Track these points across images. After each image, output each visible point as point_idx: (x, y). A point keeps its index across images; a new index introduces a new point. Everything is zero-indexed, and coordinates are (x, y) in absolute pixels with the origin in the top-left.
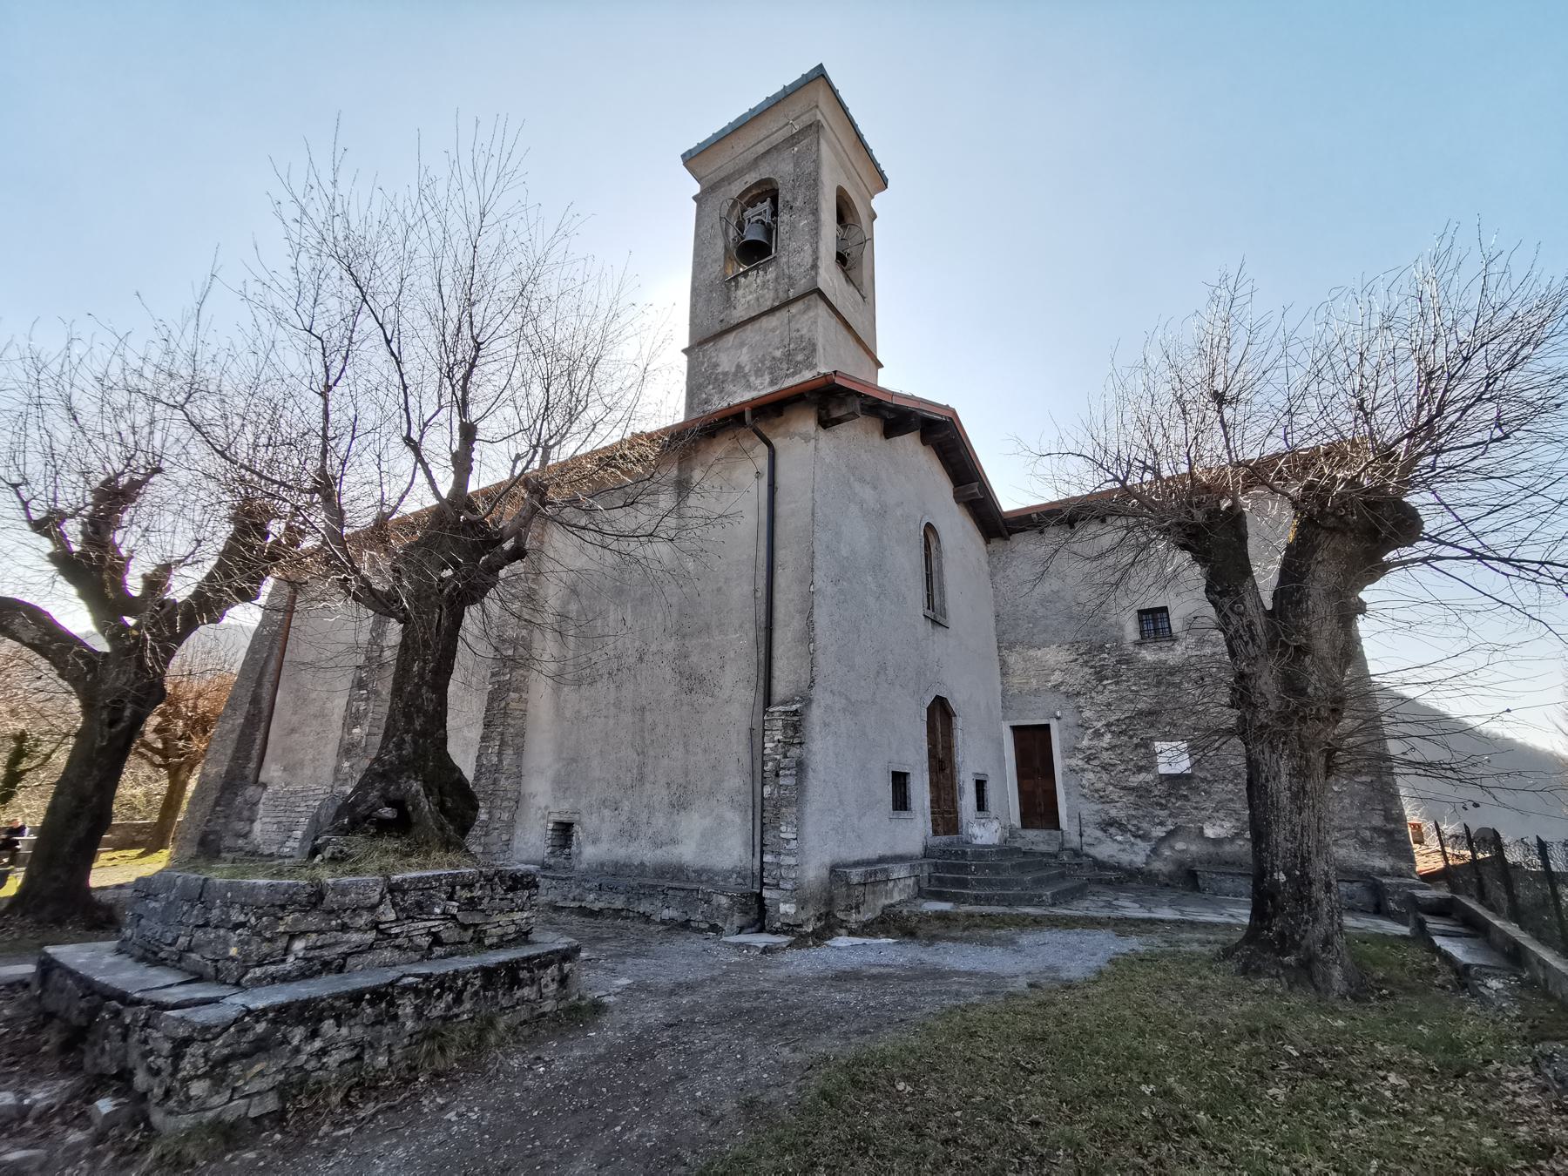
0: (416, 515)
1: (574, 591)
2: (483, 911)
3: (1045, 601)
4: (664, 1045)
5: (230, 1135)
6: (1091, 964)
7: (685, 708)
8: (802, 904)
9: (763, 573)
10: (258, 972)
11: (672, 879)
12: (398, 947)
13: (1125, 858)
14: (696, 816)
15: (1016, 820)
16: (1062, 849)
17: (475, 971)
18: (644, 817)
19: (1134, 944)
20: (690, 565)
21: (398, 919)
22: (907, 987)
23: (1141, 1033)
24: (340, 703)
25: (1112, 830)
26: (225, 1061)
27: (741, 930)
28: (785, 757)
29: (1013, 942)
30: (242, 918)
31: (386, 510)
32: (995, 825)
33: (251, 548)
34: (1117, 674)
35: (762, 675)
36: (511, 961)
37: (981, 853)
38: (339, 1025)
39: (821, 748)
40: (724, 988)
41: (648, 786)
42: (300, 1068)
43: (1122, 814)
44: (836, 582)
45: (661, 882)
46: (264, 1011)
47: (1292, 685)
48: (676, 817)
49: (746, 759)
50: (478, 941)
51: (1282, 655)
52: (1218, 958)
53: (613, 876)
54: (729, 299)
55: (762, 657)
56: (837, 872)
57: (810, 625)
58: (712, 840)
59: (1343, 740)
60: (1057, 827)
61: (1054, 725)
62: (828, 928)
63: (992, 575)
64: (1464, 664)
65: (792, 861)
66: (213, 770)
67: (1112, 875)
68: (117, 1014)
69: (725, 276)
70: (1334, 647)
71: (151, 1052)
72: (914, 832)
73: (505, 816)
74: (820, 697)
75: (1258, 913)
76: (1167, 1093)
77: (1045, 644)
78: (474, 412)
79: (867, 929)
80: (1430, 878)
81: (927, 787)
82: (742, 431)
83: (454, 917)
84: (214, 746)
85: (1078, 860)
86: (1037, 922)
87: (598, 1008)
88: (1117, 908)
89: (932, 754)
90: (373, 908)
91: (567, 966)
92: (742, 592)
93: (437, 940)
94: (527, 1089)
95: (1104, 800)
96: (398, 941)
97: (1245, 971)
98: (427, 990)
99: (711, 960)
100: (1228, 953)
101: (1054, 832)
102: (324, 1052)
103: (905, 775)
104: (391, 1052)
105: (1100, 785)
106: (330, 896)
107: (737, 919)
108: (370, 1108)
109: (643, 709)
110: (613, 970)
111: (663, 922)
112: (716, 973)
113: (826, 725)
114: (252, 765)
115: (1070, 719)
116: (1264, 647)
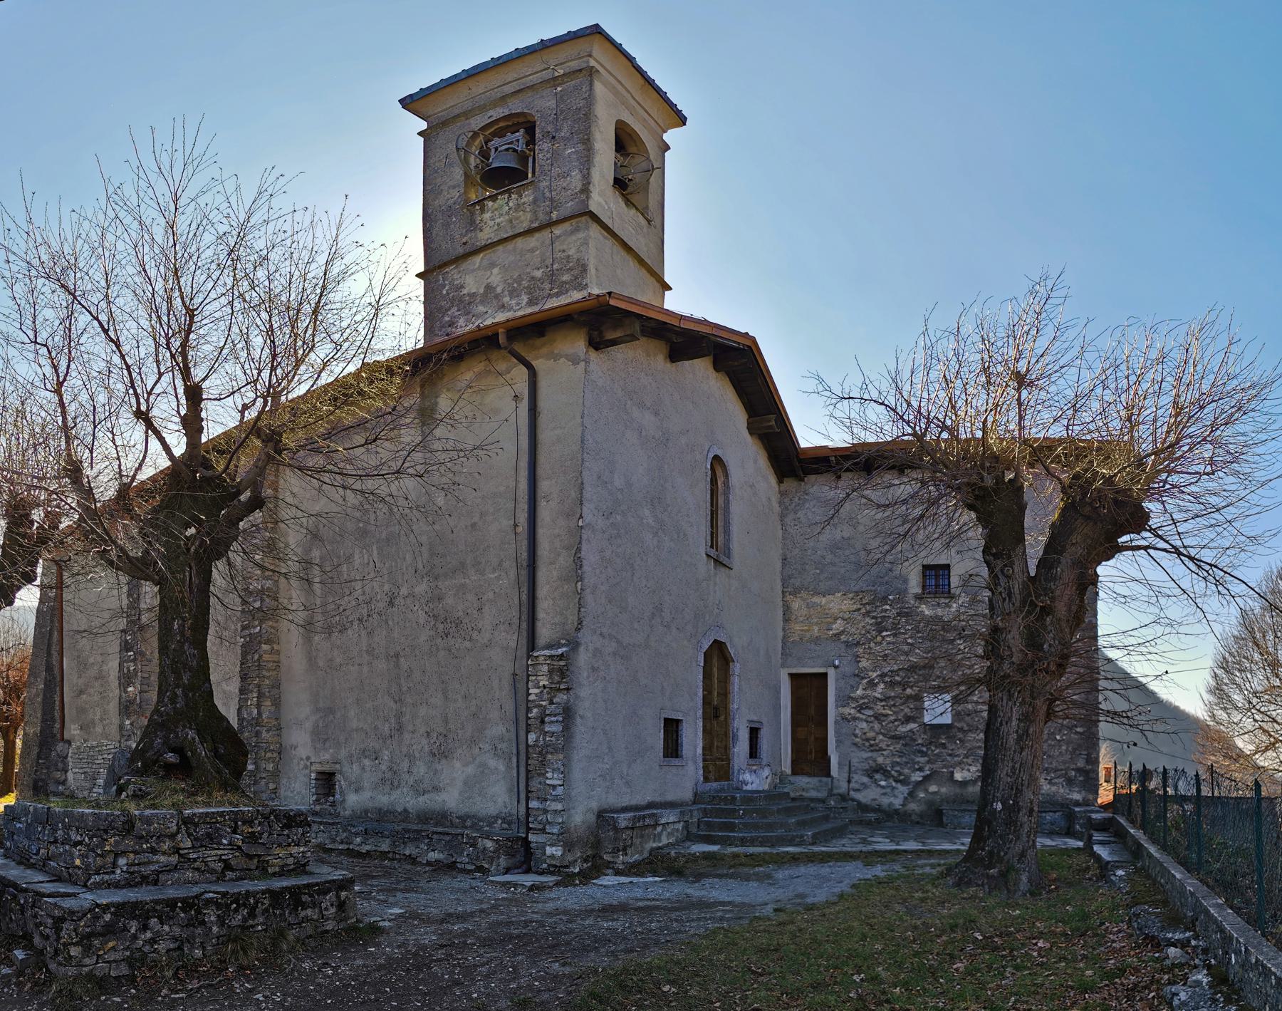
0: (153, 479)
1: (315, 536)
2: (263, 844)
3: (834, 547)
4: (439, 960)
5: (102, 984)
6: (835, 890)
7: (442, 653)
8: (569, 847)
9: (524, 505)
10: (98, 878)
11: (436, 825)
12: (198, 869)
13: (885, 801)
14: (458, 764)
15: (787, 768)
16: (831, 794)
17: (263, 892)
18: (405, 765)
19: (879, 871)
20: (440, 500)
21: (193, 847)
22: (673, 916)
23: (864, 937)
24: (113, 665)
25: (878, 776)
26: (89, 936)
27: (507, 871)
28: (551, 703)
29: (769, 876)
30: (79, 838)
31: (125, 480)
32: (767, 772)
33: (24, 536)
34: (895, 627)
35: (524, 617)
36: (293, 887)
37: (751, 797)
38: (162, 924)
39: (588, 695)
40: (493, 918)
41: (407, 736)
42: (140, 950)
43: (888, 761)
44: (608, 515)
45: (425, 827)
46: (108, 906)
47: (1033, 640)
48: (439, 767)
49: (509, 707)
50: (263, 870)
51: (1029, 613)
52: (942, 875)
53: (377, 821)
54: (472, 222)
55: (524, 597)
56: (604, 817)
57: (578, 562)
58: (474, 784)
59: (1062, 691)
60: (828, 775)
61: (832, 674)
62: (595, 868)
63: (782, 517)
64: (1148, 633)
65: (559, 807)
66: (31, 731)
67: (872, 816)
68: (15, 897)
69: (466, 201)
70: (1069, 610)
71: (41, 924)
72: (687, 777)
73: (270, 767)
74: (588, 639)
75: (978, 839)
76: (875, 979)
77: (830, 592)
78: (198, 373)
79: (633, 869)
80: (1105, 807)
81: (700, 734)
82: (495, 355)
83: (239, 848)
84: (27, 709)
85: (844, 804)
86: (795, 859)
87: (375, 930)
88: (870, 843)
89: (707, 701)
90: (172, 836)
91: (343, 894)
92: (501, 528)
93: (227, 866)
94: (319, 984)
95: (876, 749)
96: (196, 864)
97: (958, 885)
98: (225, 904)
99: (479, 896)
100: (949, 871)
101: (824, 779)
102: (153, 941)
103: (678, 722)
104: (204, 948)
105: (871, 734)
106: (138, 824)
107: (503, 861)
108: (195, 984)
109: (397, 655)
110: (385, 901)
111: (429, 863)
112: (484, 906)
113: (594, 669)
114: (57, 726)
115: (848, 669)
116: (1017, 604)
